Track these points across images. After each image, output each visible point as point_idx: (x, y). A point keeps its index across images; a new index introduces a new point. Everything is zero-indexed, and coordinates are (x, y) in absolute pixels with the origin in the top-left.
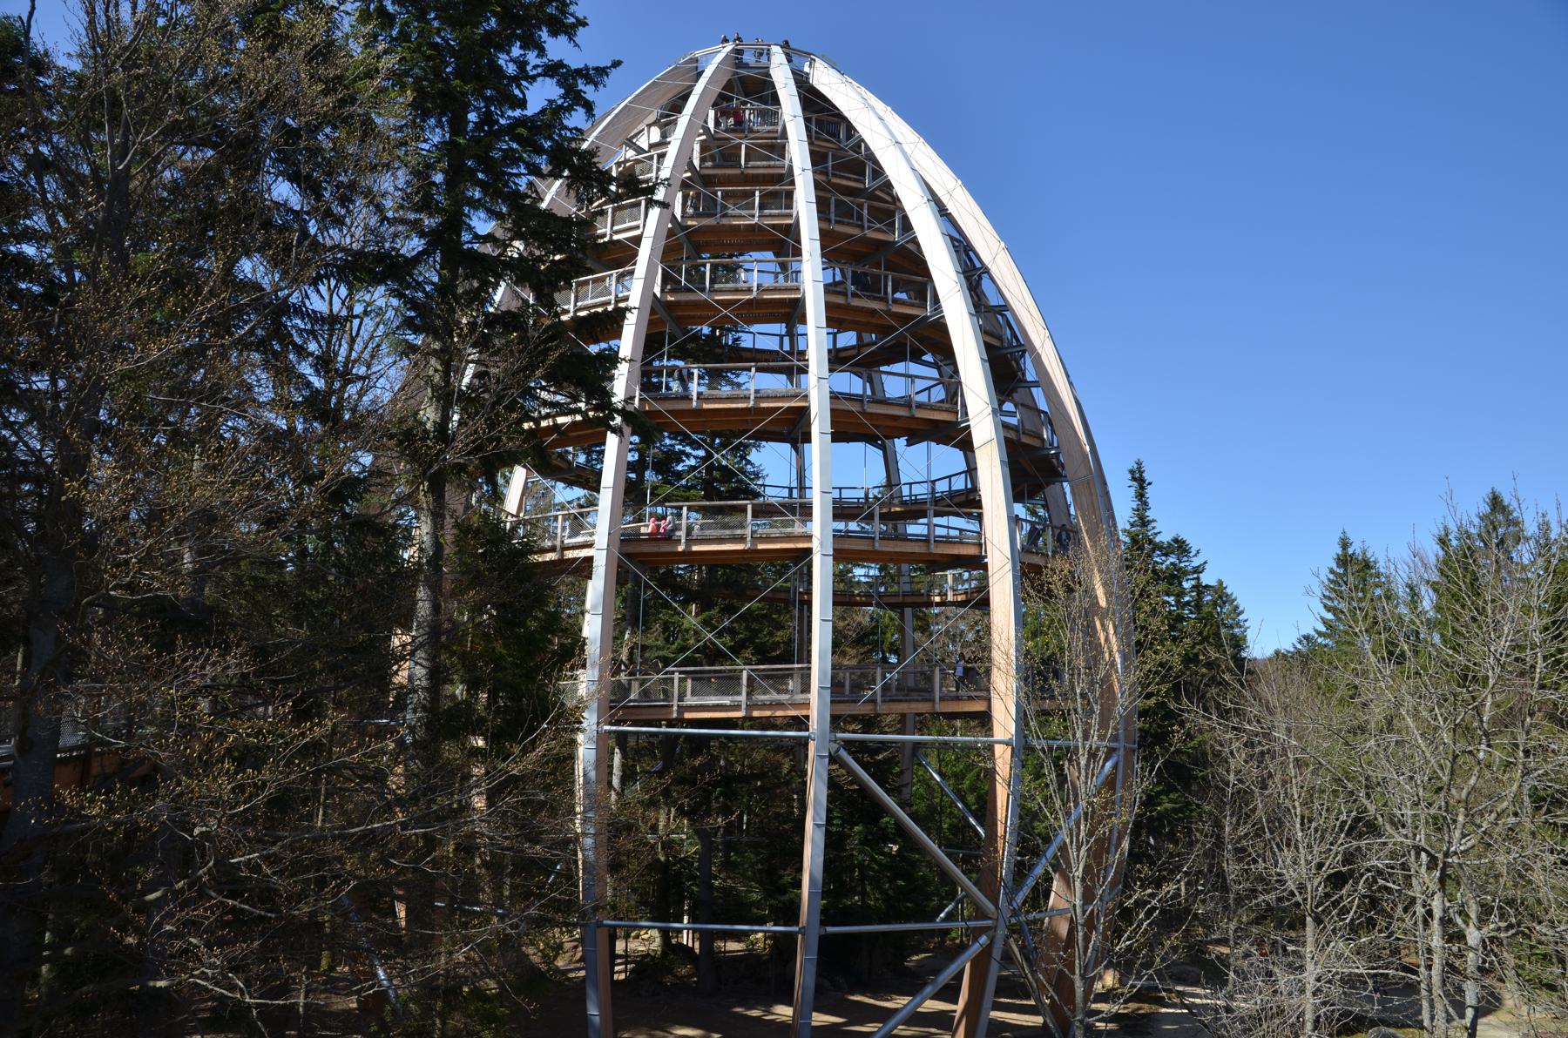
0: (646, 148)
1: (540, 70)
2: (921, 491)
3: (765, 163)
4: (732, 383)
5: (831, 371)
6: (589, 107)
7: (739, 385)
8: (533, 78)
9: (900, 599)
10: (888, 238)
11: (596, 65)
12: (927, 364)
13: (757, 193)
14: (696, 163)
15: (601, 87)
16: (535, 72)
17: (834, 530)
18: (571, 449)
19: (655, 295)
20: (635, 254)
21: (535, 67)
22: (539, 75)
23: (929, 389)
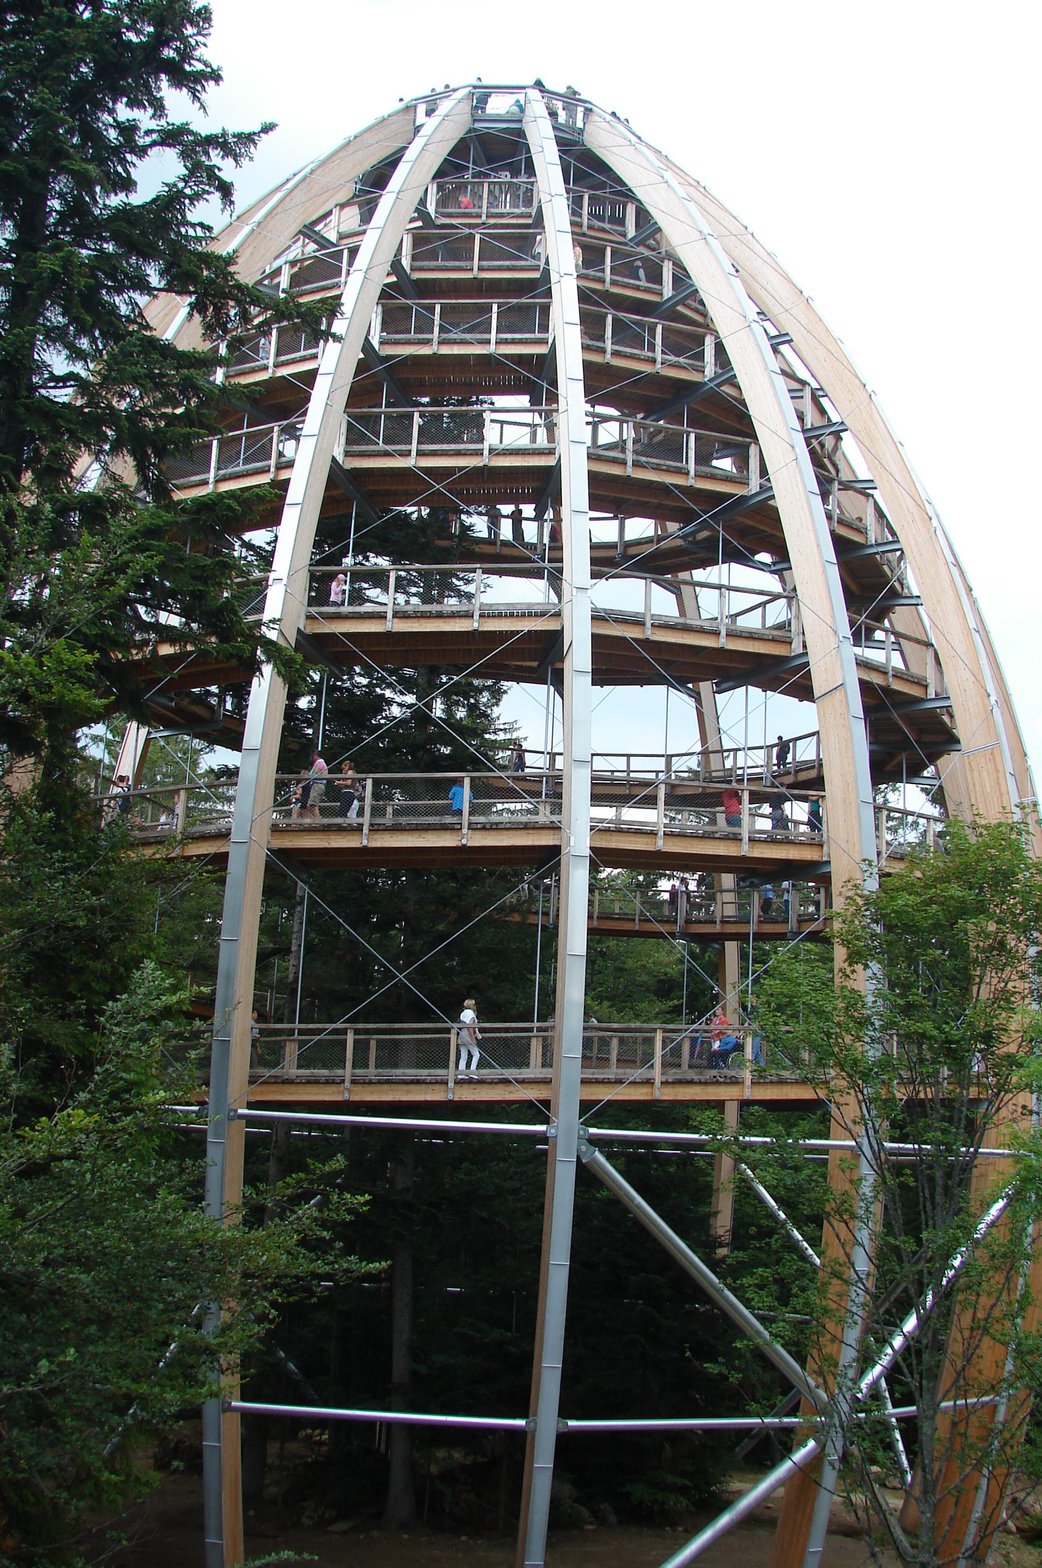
0: (334, 240)
1: (155, 136)
2: (754, 762)
3: (507, 263)
4: (459, 594)
5: (595, 575)
6: (226, 190)
7: (469, 596)
8: (142, 152)
9: (717, 928)
10: (694, 377)
11: (238, 130)
12: (762, 567)
13: (495, 308)
14: (406, 262)
15: (245, 162)
16: (148, 140)
17: (592, 820)
18: (214, 689)
19: (334, 459)
20: (307, 399)
21: (149, 132)
22: (154, 144)
23: (763, 605)
